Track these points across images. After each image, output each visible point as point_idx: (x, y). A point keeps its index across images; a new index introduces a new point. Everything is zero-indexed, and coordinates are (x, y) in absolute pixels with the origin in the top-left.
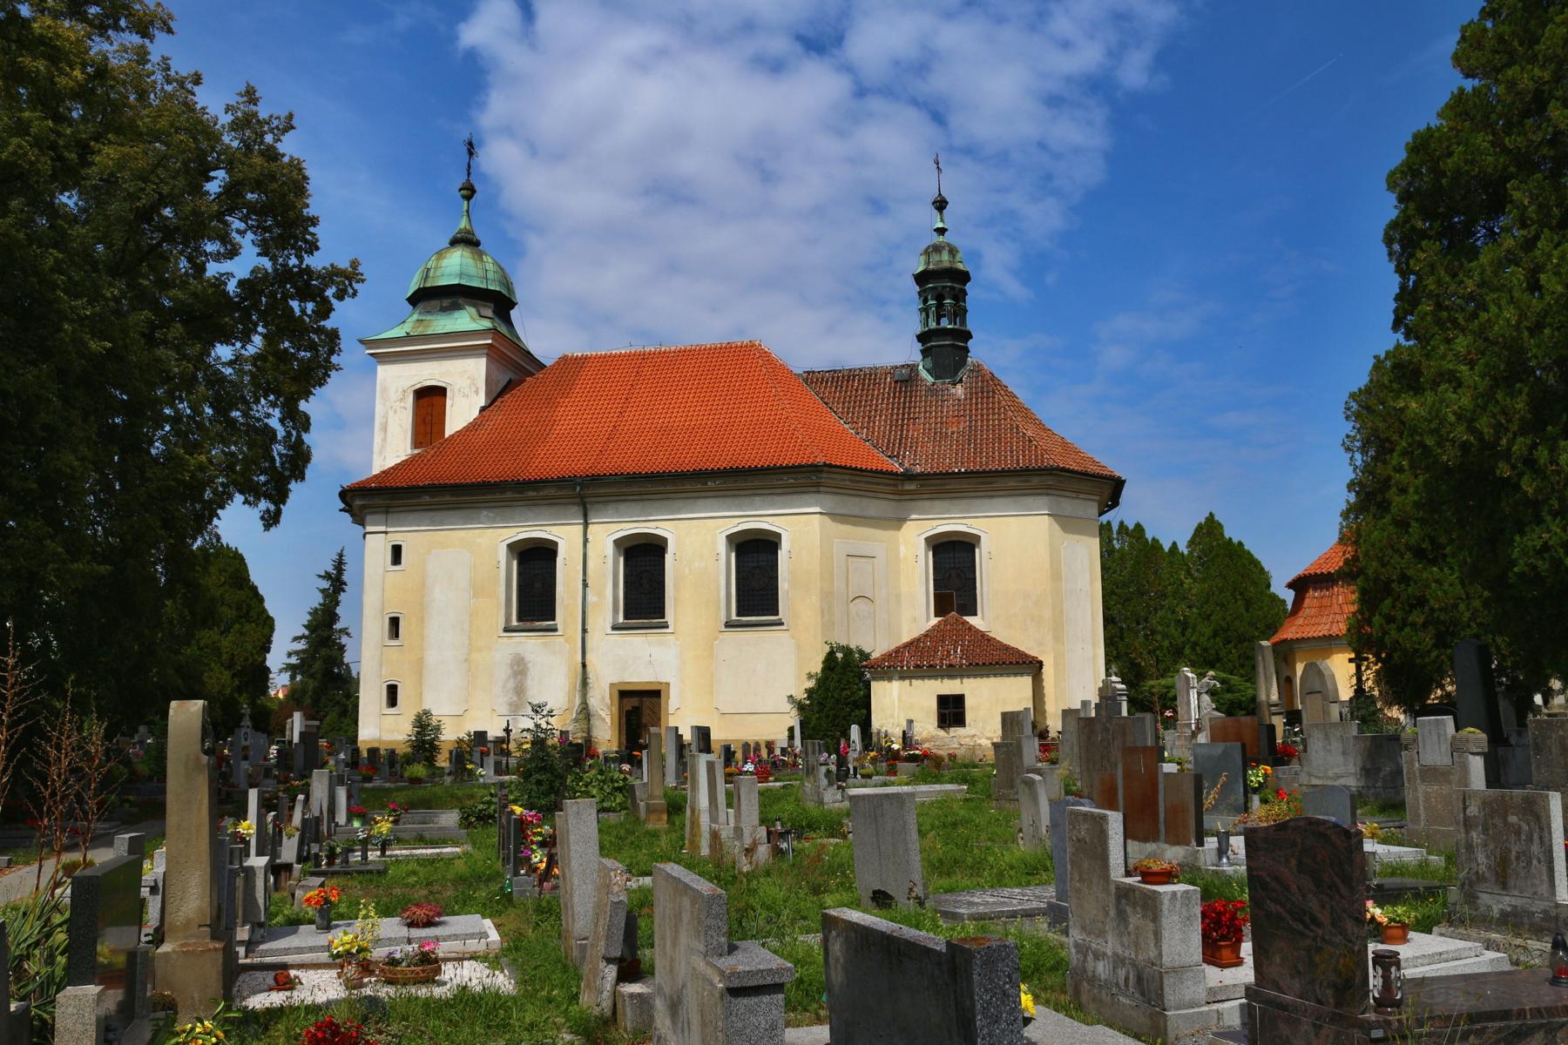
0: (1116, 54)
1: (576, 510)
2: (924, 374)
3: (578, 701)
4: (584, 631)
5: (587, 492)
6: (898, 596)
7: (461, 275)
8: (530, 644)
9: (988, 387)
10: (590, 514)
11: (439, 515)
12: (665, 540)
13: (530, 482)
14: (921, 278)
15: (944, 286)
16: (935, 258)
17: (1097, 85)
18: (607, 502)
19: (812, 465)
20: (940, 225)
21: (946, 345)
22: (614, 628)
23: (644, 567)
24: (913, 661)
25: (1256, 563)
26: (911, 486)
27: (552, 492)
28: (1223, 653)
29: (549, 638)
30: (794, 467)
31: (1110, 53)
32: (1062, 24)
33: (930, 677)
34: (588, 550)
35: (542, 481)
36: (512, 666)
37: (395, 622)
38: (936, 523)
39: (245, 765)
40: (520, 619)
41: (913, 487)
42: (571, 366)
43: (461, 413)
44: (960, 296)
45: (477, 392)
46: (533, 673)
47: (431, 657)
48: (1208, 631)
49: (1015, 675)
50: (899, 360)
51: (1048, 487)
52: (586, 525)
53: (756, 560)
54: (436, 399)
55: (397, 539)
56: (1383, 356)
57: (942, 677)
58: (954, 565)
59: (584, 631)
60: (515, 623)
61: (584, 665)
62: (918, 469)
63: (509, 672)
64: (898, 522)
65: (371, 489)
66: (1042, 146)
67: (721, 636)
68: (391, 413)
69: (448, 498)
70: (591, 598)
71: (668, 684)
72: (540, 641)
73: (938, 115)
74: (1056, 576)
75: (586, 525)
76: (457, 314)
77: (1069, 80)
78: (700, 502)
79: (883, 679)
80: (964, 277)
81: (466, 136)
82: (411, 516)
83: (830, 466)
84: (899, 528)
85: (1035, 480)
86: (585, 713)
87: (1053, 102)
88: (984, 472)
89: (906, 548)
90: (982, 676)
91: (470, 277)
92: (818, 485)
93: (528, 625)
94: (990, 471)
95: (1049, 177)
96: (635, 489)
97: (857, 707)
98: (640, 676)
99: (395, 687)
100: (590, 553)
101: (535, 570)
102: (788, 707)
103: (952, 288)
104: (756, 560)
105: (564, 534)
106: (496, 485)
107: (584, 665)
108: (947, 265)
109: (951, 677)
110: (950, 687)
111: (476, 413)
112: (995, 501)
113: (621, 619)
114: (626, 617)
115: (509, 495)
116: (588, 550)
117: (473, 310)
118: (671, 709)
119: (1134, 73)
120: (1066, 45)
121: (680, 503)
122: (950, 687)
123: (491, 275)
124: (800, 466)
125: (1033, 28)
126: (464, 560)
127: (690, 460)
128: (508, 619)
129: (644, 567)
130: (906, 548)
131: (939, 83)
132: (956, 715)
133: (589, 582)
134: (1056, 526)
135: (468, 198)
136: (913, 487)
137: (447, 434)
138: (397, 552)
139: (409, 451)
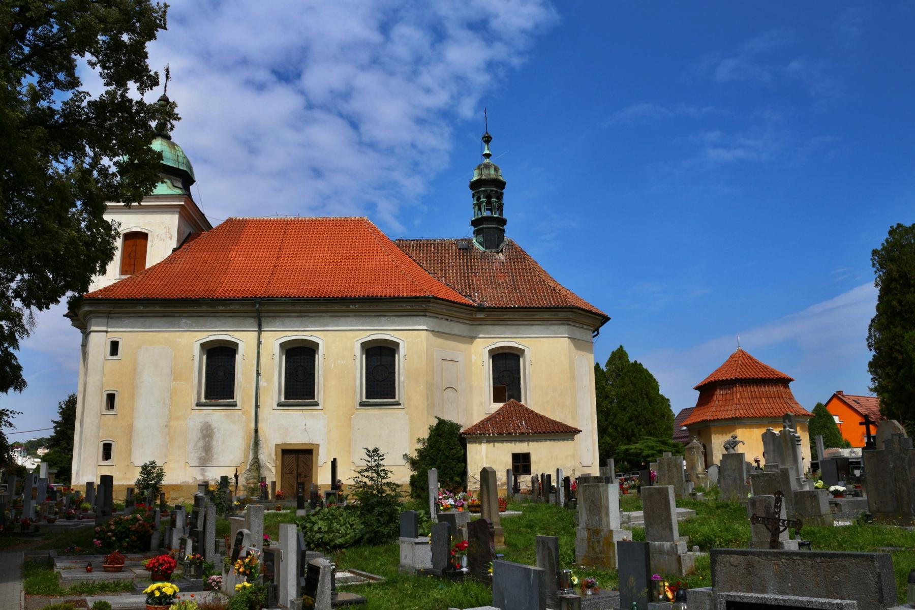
0: (457, 98)
2: (477, 245)
3: (251, 457)
4: (257, 406)
5: (266, 308)
6: (471, 388)
8: (216, 416)
9: (519, 257)
10: (263, 325)
11: (148, 321)
12: (316, 345)
13: (221, 299)
14: (474, 185)
15: (489, 190)
16: (485, 172)
17: (447, 115)
18: (275, 317)
19: (424, 297)
20: (487, 152)
23: (300, 365)
24: (488, 431)
25: (651, 376)
26: (481, 316)
27: (237, 307)
28: (636, 430)
29: (230, 412)
30: (412, 298)
31: (452, 98)
32: (426, 79)
33: (507, 441)
34: (260, 351)
35: (230, 299)
36: (202, 431)
37: (111, 398)
38: (495, 340)
39: (33, 504)
40: (206, 398)
41: (482, 316)
42: (234, 227)
44: (500, 197)
45: (171, 238)
47: (139, 424)
48: (626, 418)
49: (564, 440)
51: (568, 320)
52: (260, 332)
53: (380, 364)
55: (115, 337)
56: (895, 226)
57: (515, 441)
59: (257, 406)
60: (203, 400)
61: (256, 431)
62: (486, 304)
63: (199, 435)
64: (472, 338)
65: (98, 299)
66: (413, 146)
69: (157, 309)
70: (263, 383)
71: (318, 445)
72: (223, 413)
73: (354, 123)
74: (573, 378)
75: (260, 332)
77: (428, 110)
78: (343, 320)
79: (475, 442)
80: (501, 185)
82: (127, 321)
83: (436, 298)
84: (471, 343)
85: (561, 315)
86: (257, 465)
88: (530, 308)
89: (477, 355)
90: (541, 440)
92: (425, 311)
93: (213, 402)
94: (534, 308)
95: (416, 164)
96: (298, 308)
97: (459, 461)
98: (297, 439)
100: (262, 352)
101: (220, 363)
103: (496, 192)
104: (380, 364)
105: (244, 338)
107: (256, 431)
108: (494, 177)
109: (521, 441)
110: (521, 448)
111: (169, 253)
112: (534, 327)
113: (283, 399)
114: (286, 398)
115: (204, 308)
116: (260, 351)
119: (467, 109)
120: (428, 91)
121: (328, 320)
122: (521, 448)
124: (416, 297)
125: (409, 80)
126: (170, 352)
127: (337, 289)
129: (300, 365)
130: (477, 355)
131: (355, 105)
132: (524, 466)
133: (261, 372)
134: (572, 345)
136: (482, 316)
137: (148, 266)
138: (114, 347)
139: (118, 277)
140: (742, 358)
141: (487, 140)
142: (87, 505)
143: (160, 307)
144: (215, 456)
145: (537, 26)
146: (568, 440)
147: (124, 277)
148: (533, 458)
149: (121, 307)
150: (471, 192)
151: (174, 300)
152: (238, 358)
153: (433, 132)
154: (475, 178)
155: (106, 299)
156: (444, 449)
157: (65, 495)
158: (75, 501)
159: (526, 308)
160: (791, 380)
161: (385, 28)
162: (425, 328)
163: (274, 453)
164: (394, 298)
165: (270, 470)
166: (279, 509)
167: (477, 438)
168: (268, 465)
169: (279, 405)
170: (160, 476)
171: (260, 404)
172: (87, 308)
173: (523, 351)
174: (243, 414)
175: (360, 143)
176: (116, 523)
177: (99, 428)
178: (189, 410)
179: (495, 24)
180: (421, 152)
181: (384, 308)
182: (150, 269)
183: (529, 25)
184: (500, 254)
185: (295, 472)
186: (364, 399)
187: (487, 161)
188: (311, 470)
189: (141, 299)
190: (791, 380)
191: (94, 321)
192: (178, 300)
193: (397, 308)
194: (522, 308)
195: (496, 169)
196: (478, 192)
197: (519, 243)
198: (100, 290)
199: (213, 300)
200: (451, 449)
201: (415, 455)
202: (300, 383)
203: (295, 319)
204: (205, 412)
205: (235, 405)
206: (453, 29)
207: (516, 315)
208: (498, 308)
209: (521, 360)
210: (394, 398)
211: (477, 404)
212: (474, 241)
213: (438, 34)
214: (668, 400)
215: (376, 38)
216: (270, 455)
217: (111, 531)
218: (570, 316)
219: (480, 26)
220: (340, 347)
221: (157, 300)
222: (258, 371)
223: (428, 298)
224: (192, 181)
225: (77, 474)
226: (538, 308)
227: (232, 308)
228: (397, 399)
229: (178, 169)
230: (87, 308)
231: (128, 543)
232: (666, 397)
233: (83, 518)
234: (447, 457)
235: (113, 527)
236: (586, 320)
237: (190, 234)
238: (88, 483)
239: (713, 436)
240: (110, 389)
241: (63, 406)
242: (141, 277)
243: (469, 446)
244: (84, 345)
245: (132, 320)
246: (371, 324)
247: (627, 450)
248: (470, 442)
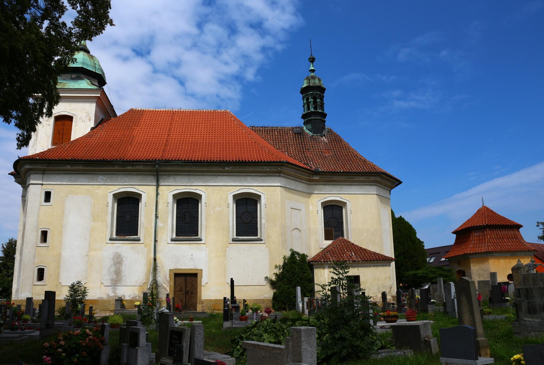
0: (243, 68)
3: (151, 279)
4: (156, 241)
5: (162, 168)
7: (83, 63)
8: (124, 248)
9: (336, 139)
13: (130, 161)
14: (304, 91)
15: (314, 94)
16: (312, 81)
17: (238, 78)
18: (169, 175)
19: (280, 162)
21: (315, 118)
22: (172, 240)
25: (411, 226)
27: (141, 168)
29: (135, 245)
31: (241, 68)
32: (225, 57)
34: (157, 201)
35: (137, 161)
36: (114, 259)
37: (44, 234)
40: (117, 234)
44: (322, 99)
45: (90, 120)
49: (383, 266)
50: (294, 125)
51: (377, 182)
52: (158, 186)
54: (66, 122)
55: (48, 188)
58: (334, 214)
59: (156, 241)
60: (114, 236)
61: (155, 260)
63: (112, 262)
65: (37, 160)
66: (218, 96)
67: (230, 245)
69: (81, 167)
70: (160, 224)
71: (201, 270)
72: (130, 246)
73: (182, 82)
75: (158, 186)
76: (80, 82)
77: (226, 75)
79: (320, 268)
80: (323, 90)
82: (58, 177)
84: (309, 197)
85: (372, 178)
86: (155, 285)
87: (221, 82)
90: (368, 266)
92: (280, 172)
93: (122, 237)
94: (354, 173)
96: (187, 169)
98: (186, 266)
99: (43, 269)
100: (160, 201)
102: (265, 283)
103: (320, 95)
105: (146, 191)
106: (111, 161)
107: (155, 260)
108: (319, 84)
111: (89, 130)
113: (174, 236)
114: (176, 235)
115: (117, 168)
116: (157, 201)
117: (88, 81)
118: (203, 283)
119: (250, 75)
120: (226, 63)
121: (243, 178)
124: (274, 162)
125: (215, 57)
127: (215, 155)
128: (112, 234)
131: (182, 71)
133: (159, 215)
134: (379, 200)
137: (72, 139)
138: (48, 196)
140: (485, 212)
141: (312, 60)
142: (27, 317)
143: (83, 166)
144: (124, 278)
145: (291, 27)
146: (386, 266)
147: (54, 147)
148: (362, 279)
150: (301, 96)
151: (94, 161)
152: (142, 205)
153: (229, 88)
154: (305, 86)
155: (43, 160)
156: (295, 272)
157: (9, 308)
158: (17, 313)
159: (348, 173)
160: (521, 226)
161: (200, 26)
162: (279, 185)
163: (168, 276)
164: (258, 162)
165: (166, 289)
166: (191, 320)
167: (322, 264)
168: (164, 285)
169: (172, 240)
170: (84, 293)
172: (27, 167)
173: (345, 204)
174: (145, 246)
175: (186, 94)
176: (65, 338)
177: (35, 257)
178: (105, 243)
179: (267, 25)
180: (222, 100)
181: (250, 169)
182: (74, 141)
183: (287, 26)
184: (324, 137)
185: (184, 290)
186: (235, 237)
187: (313, 74)
188: (196, 288)
189: (69, 160)
190: (521, 226)
191: (32, 176)
192: (97, 161)
193: (260, 169)
194: (346, 172)
195: (319, 80)
196: (307, 95)
197: (336, 130)
198: (38, 154)
199: (124, 161)
200: (304, 273)
201: (274, 278)
202: (187, 224)
203: (184, 177)
205: (139, 240)
206: (241, 27)
207: (341, 178)
208: (329, 172)
209: (344, 210)
210: (257, 235)
211: (314, 243)
212: (305, 128)
213: (232, 30)
214: (423, 242)
215: (195, 31)
216: (166, 277)
217: (61, 347)
218: (379, 179)
219: (258, 26)
220: (217, 199)
221: (81, 160)
222: (156, 215)
223: (283, 162)
224: (105, 83)
225: (17, 291)
226: (357, 173)
228: (259, 236)
229: (95, 73)
230: (27, 167)
231: (78, 359)
232: (421, 240)
233: (25, 329)
234: (301, 279)
235: (62, 343)
236: (387, 182)
237: (103, 119)
238: (28, 299)
239: (471, 265)
240: (44, 227)
241: (5, 247)
242: (68, 146)
243: (316, 271)
244: (24, 196)
245: (61, 176)
246: (240, 181)
247: (415, 274)
248: (316, 268)
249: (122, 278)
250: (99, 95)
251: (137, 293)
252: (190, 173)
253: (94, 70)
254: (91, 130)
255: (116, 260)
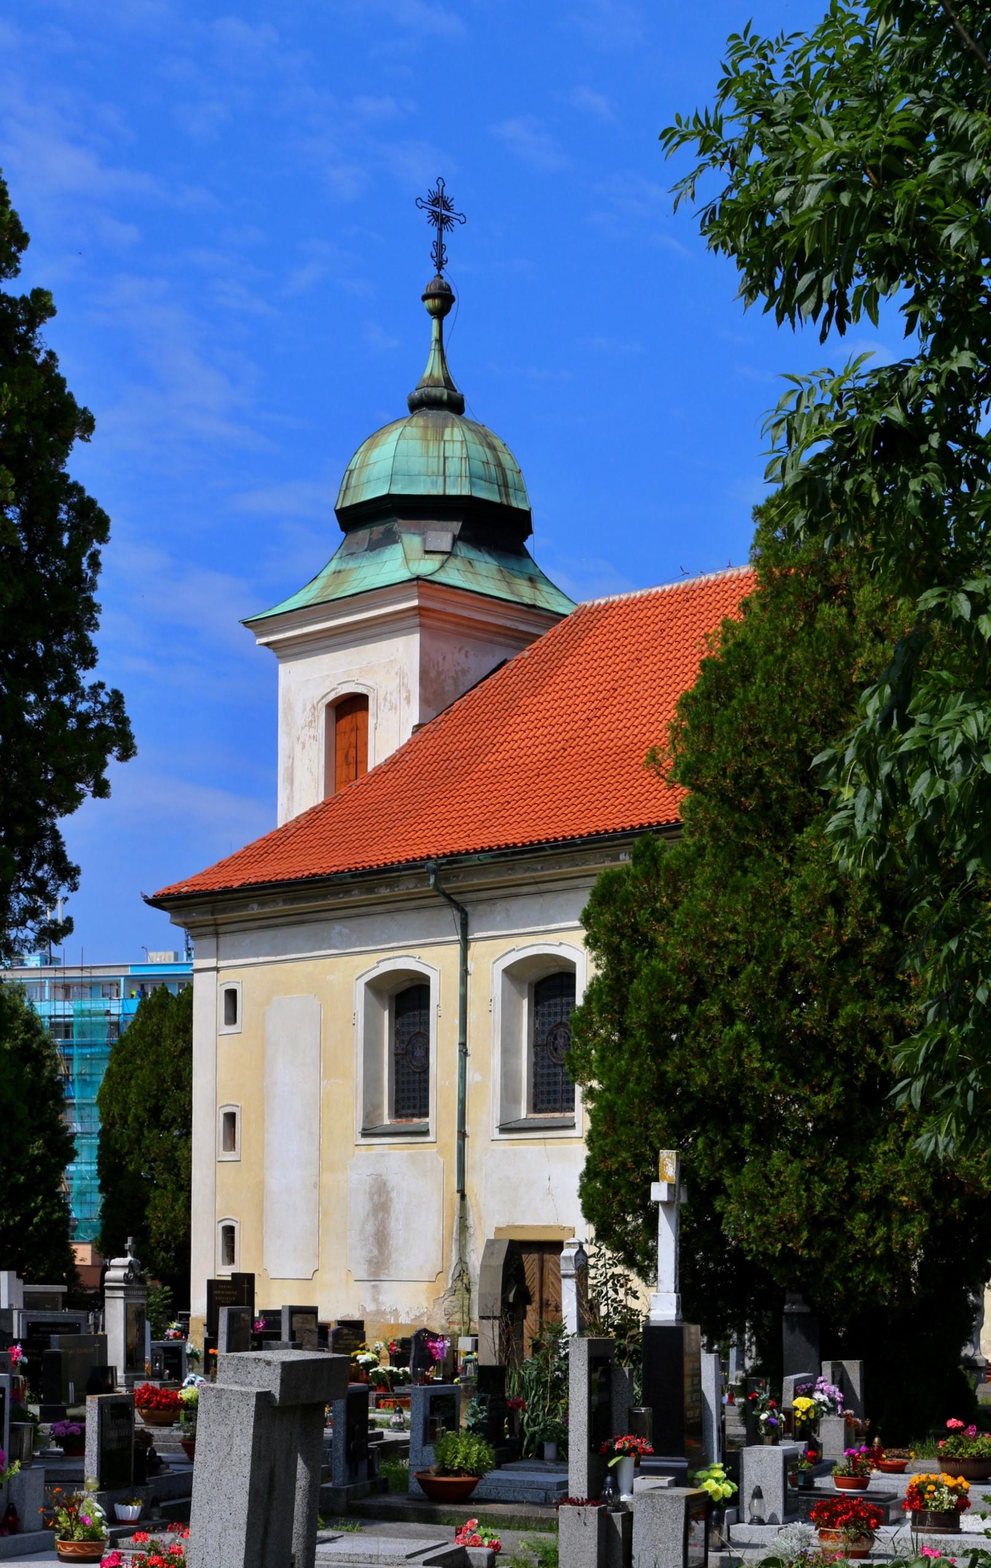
1: (451, 916)
3: (454, 1259)
4: (462, 1135)
8: (394, 1157)
10: (473, 923)
36: (371, 1195)
40: (536, 1106)
43: (389, 732)
45: (408, 700)
46: (398, 1206)
47: (274, 1184)
59: (462, 1135)
68: (298, 747)
69: (281, 907)
70: (472, 1076)
72: (406, 1152)
81: (426, 187)
91: (409, 476)
105: (434, 960)
111: (407, 735)
123: (453, 467)
128: (370, 1111)
135: (440, 314)
143: (262, 904)
144: (394, 1256)
149: (325, 897)
171: (468, 1129)
174: (440, 1152)
204: (377, 1150)
222: (463, 1044)
227: (401, 890)
245: (413, 919)
249: (390, 1255)
250: (415, 603)
251: (425, 1305)
252: (543, 887)
253: (437, 491)
254: (413, 733)
255: (376, 1197)
